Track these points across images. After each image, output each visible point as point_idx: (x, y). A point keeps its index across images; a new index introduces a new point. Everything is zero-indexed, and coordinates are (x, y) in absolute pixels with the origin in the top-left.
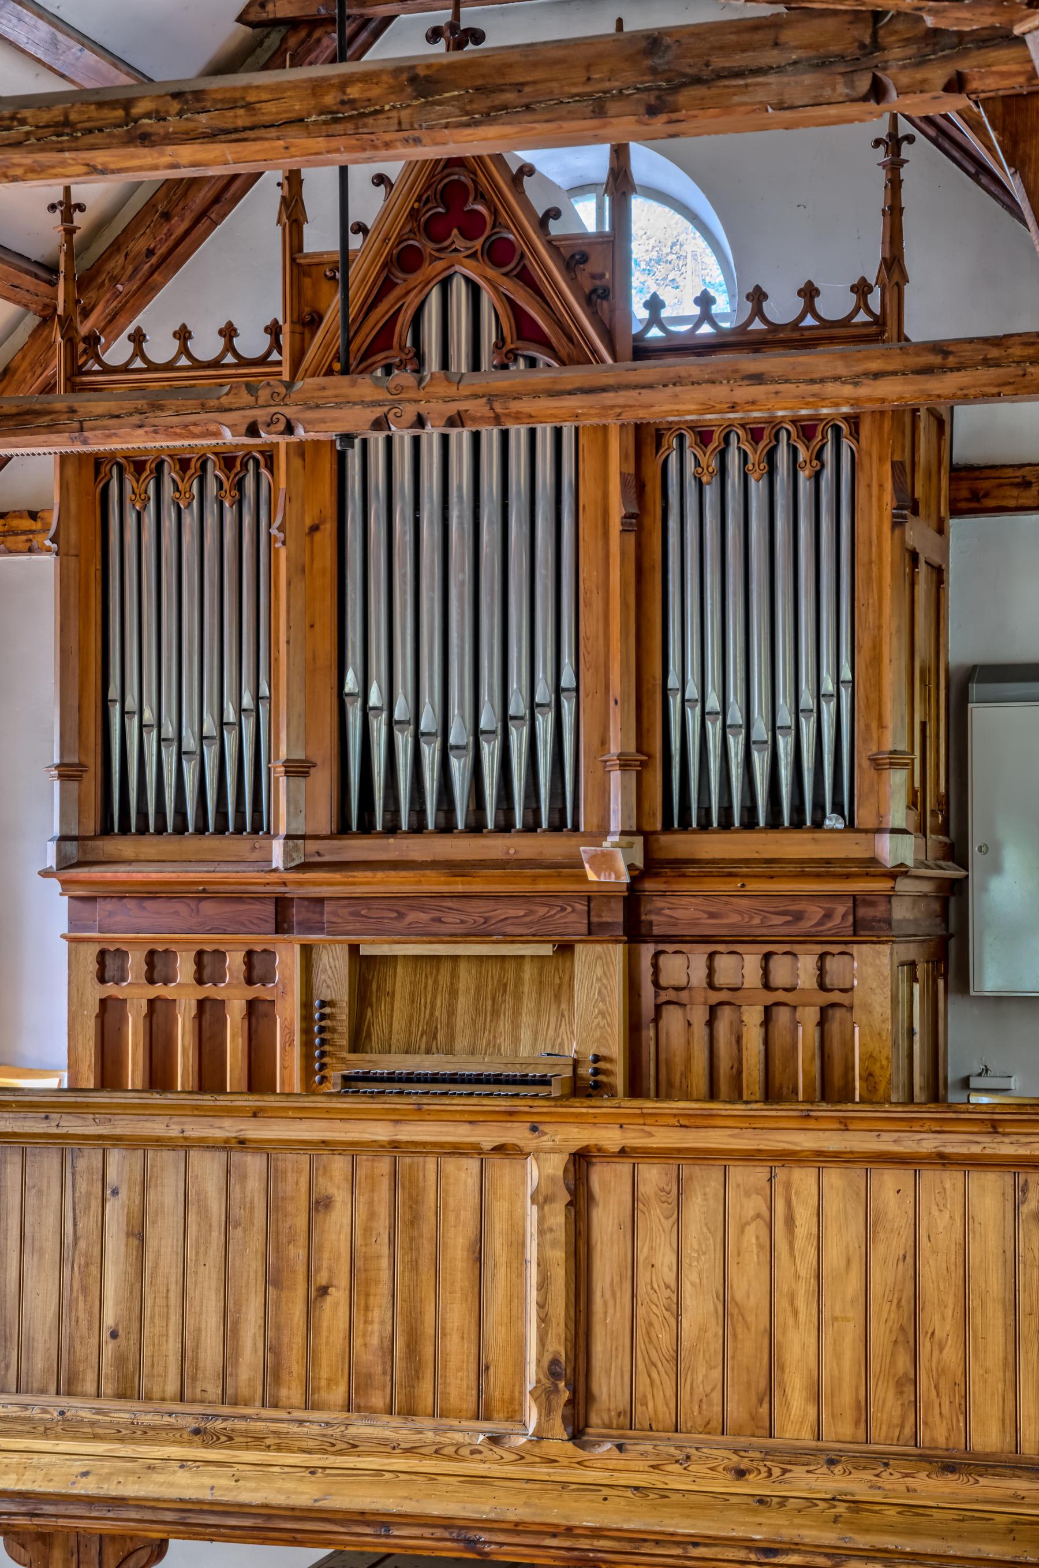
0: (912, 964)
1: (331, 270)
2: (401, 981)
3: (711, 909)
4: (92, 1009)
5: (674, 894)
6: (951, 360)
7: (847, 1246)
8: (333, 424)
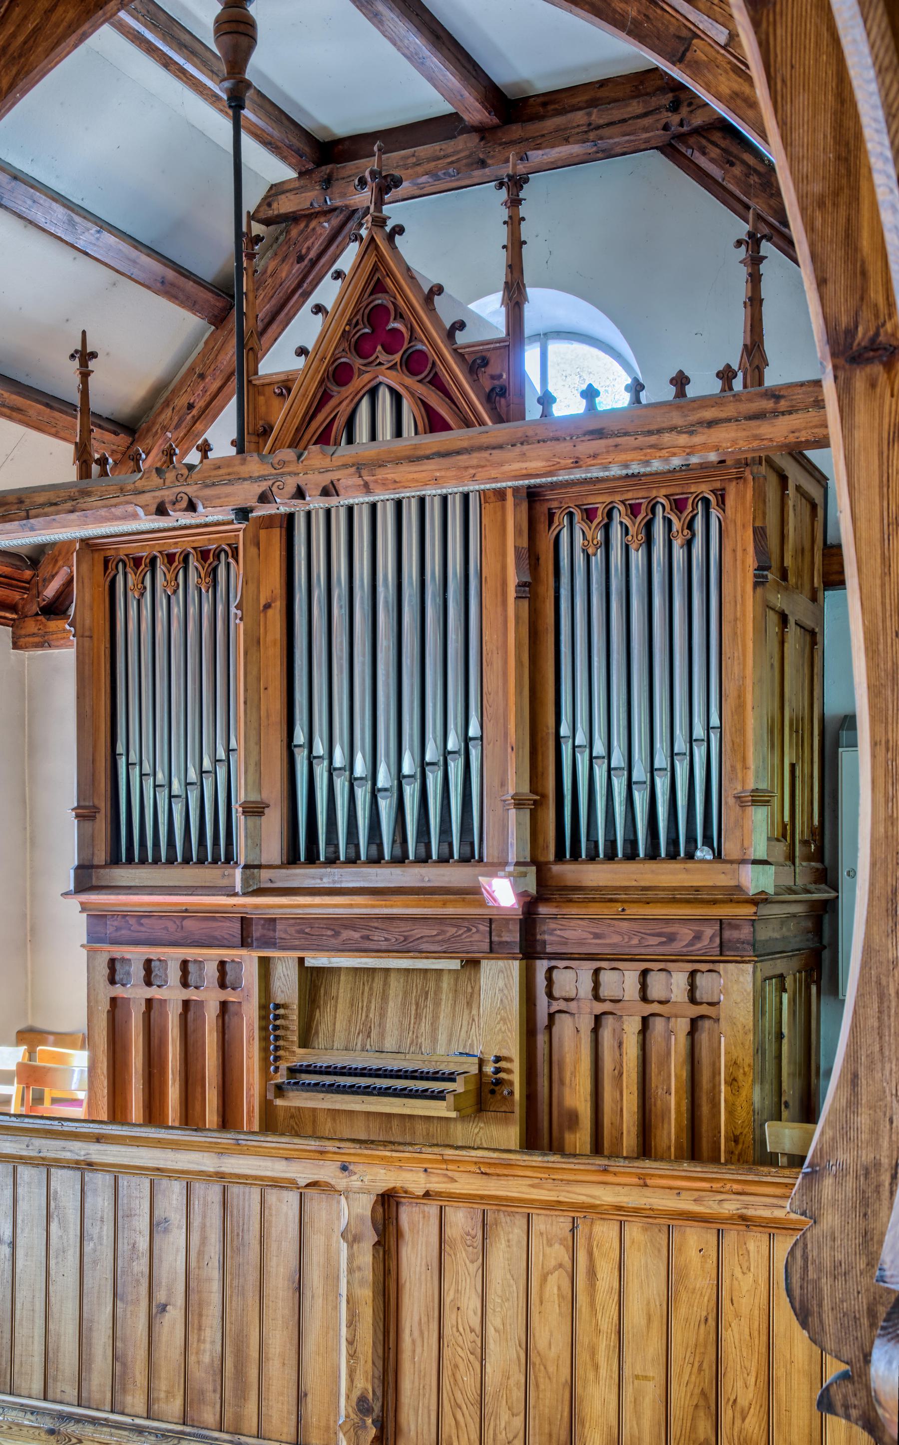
0: (781, 977)
1: (278, 388)
2: (342, 990)
3: (597, 931)
4: (104, 1006)
5: (564, 917)
6: (783, 405)
7: (648, 1304)
8: (226, 499)
